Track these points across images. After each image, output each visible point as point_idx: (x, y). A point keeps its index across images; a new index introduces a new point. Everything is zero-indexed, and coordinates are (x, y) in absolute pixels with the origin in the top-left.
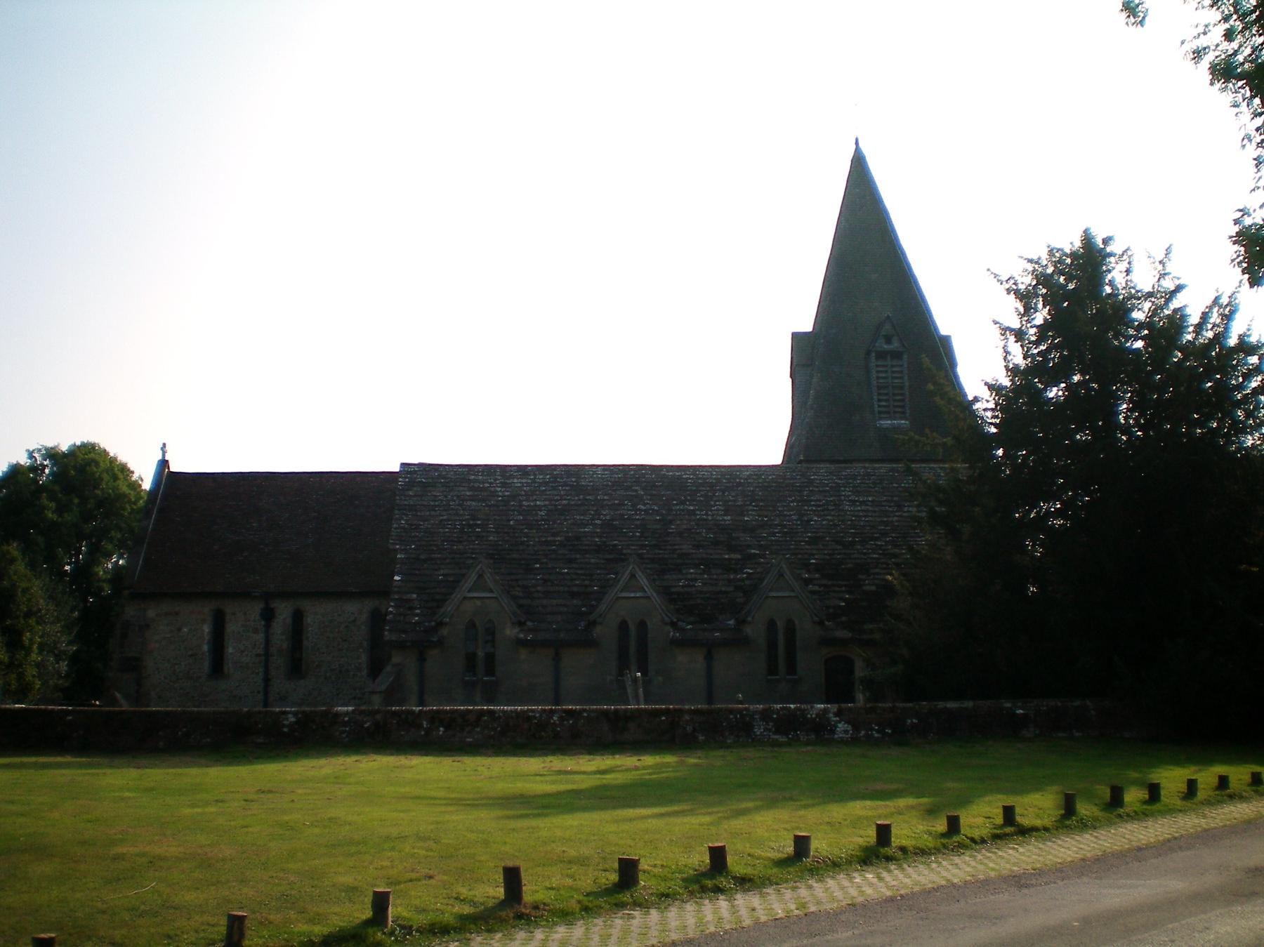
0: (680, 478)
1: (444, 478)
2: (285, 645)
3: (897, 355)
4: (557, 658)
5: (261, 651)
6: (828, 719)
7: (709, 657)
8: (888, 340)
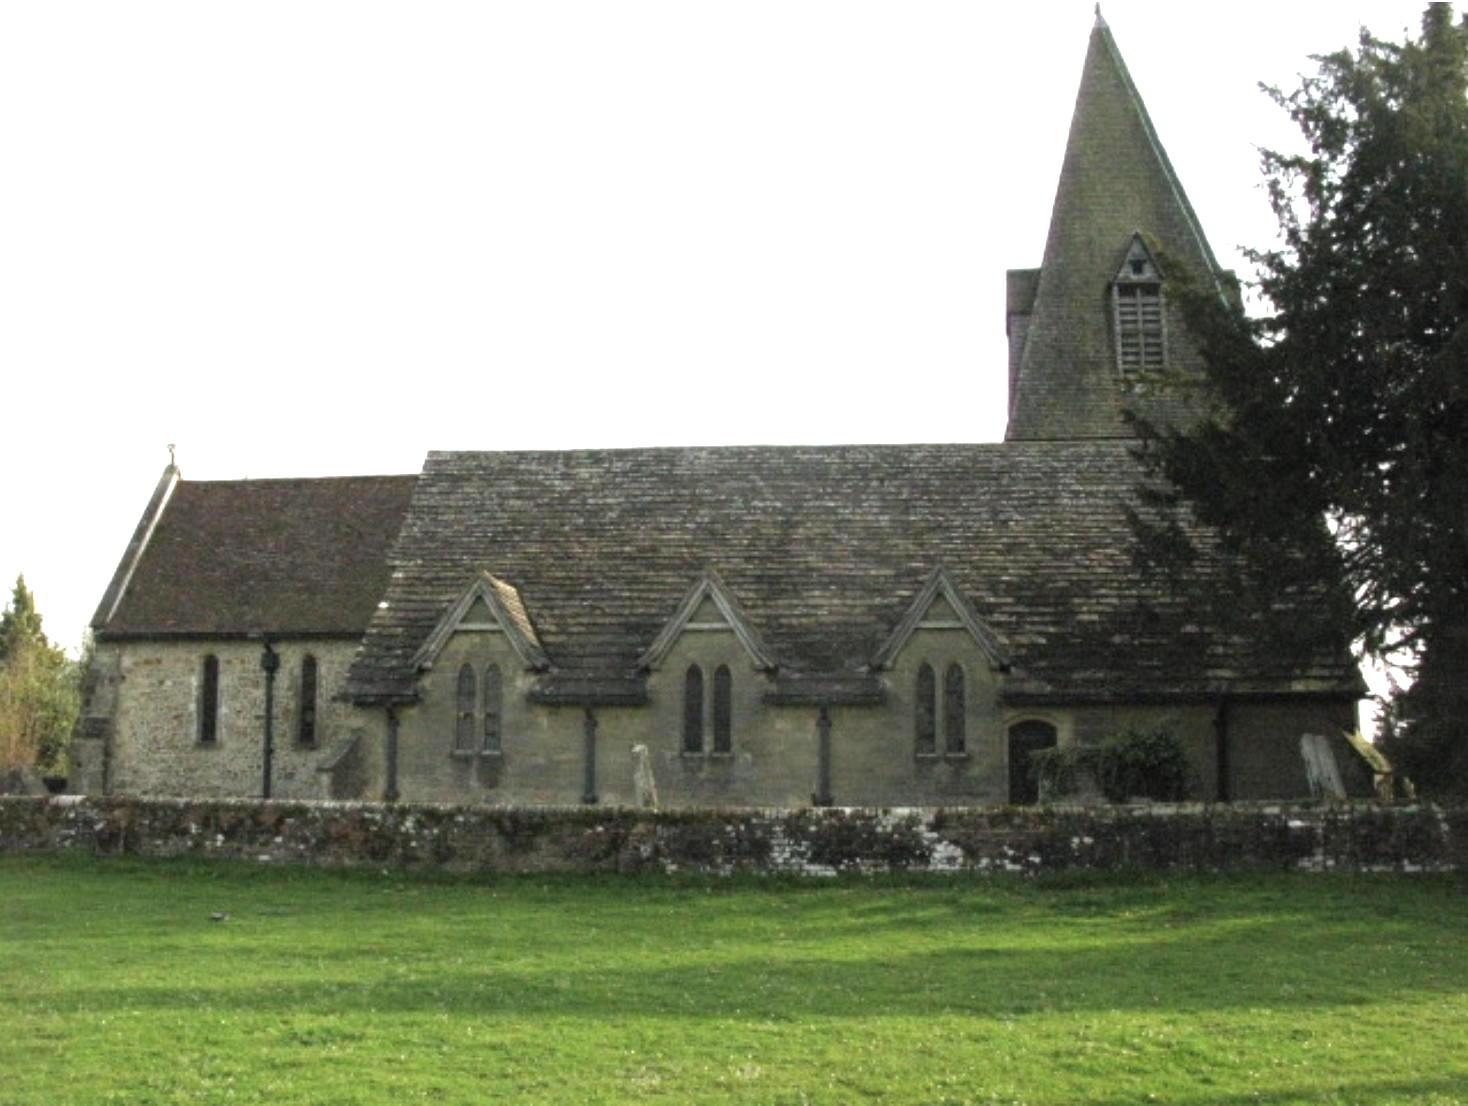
0: (819, 462)
1: (484, 469)
2: (292, 705)
3: (1150, 289)
4: (591, 724)
5: (262, 713)
6: (917, 836)
7: (825, 724)
8: (1137, 267)
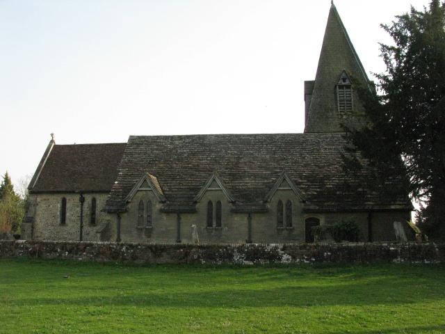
3: (348, 87)
4: (179, 219)
6: (277, 252)
7: (250, 218)
8: (344, 80)
